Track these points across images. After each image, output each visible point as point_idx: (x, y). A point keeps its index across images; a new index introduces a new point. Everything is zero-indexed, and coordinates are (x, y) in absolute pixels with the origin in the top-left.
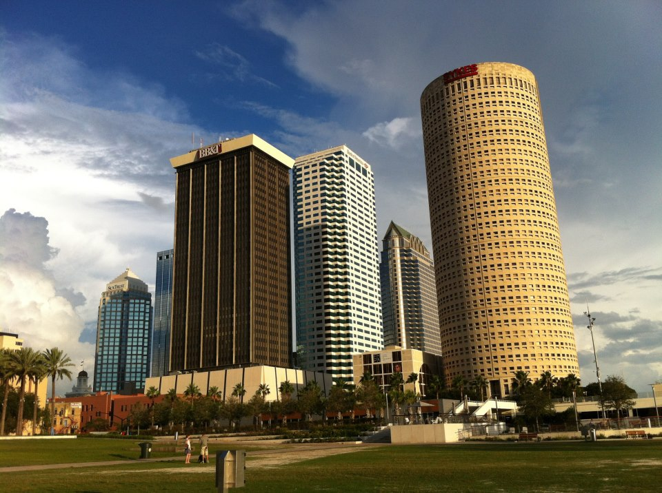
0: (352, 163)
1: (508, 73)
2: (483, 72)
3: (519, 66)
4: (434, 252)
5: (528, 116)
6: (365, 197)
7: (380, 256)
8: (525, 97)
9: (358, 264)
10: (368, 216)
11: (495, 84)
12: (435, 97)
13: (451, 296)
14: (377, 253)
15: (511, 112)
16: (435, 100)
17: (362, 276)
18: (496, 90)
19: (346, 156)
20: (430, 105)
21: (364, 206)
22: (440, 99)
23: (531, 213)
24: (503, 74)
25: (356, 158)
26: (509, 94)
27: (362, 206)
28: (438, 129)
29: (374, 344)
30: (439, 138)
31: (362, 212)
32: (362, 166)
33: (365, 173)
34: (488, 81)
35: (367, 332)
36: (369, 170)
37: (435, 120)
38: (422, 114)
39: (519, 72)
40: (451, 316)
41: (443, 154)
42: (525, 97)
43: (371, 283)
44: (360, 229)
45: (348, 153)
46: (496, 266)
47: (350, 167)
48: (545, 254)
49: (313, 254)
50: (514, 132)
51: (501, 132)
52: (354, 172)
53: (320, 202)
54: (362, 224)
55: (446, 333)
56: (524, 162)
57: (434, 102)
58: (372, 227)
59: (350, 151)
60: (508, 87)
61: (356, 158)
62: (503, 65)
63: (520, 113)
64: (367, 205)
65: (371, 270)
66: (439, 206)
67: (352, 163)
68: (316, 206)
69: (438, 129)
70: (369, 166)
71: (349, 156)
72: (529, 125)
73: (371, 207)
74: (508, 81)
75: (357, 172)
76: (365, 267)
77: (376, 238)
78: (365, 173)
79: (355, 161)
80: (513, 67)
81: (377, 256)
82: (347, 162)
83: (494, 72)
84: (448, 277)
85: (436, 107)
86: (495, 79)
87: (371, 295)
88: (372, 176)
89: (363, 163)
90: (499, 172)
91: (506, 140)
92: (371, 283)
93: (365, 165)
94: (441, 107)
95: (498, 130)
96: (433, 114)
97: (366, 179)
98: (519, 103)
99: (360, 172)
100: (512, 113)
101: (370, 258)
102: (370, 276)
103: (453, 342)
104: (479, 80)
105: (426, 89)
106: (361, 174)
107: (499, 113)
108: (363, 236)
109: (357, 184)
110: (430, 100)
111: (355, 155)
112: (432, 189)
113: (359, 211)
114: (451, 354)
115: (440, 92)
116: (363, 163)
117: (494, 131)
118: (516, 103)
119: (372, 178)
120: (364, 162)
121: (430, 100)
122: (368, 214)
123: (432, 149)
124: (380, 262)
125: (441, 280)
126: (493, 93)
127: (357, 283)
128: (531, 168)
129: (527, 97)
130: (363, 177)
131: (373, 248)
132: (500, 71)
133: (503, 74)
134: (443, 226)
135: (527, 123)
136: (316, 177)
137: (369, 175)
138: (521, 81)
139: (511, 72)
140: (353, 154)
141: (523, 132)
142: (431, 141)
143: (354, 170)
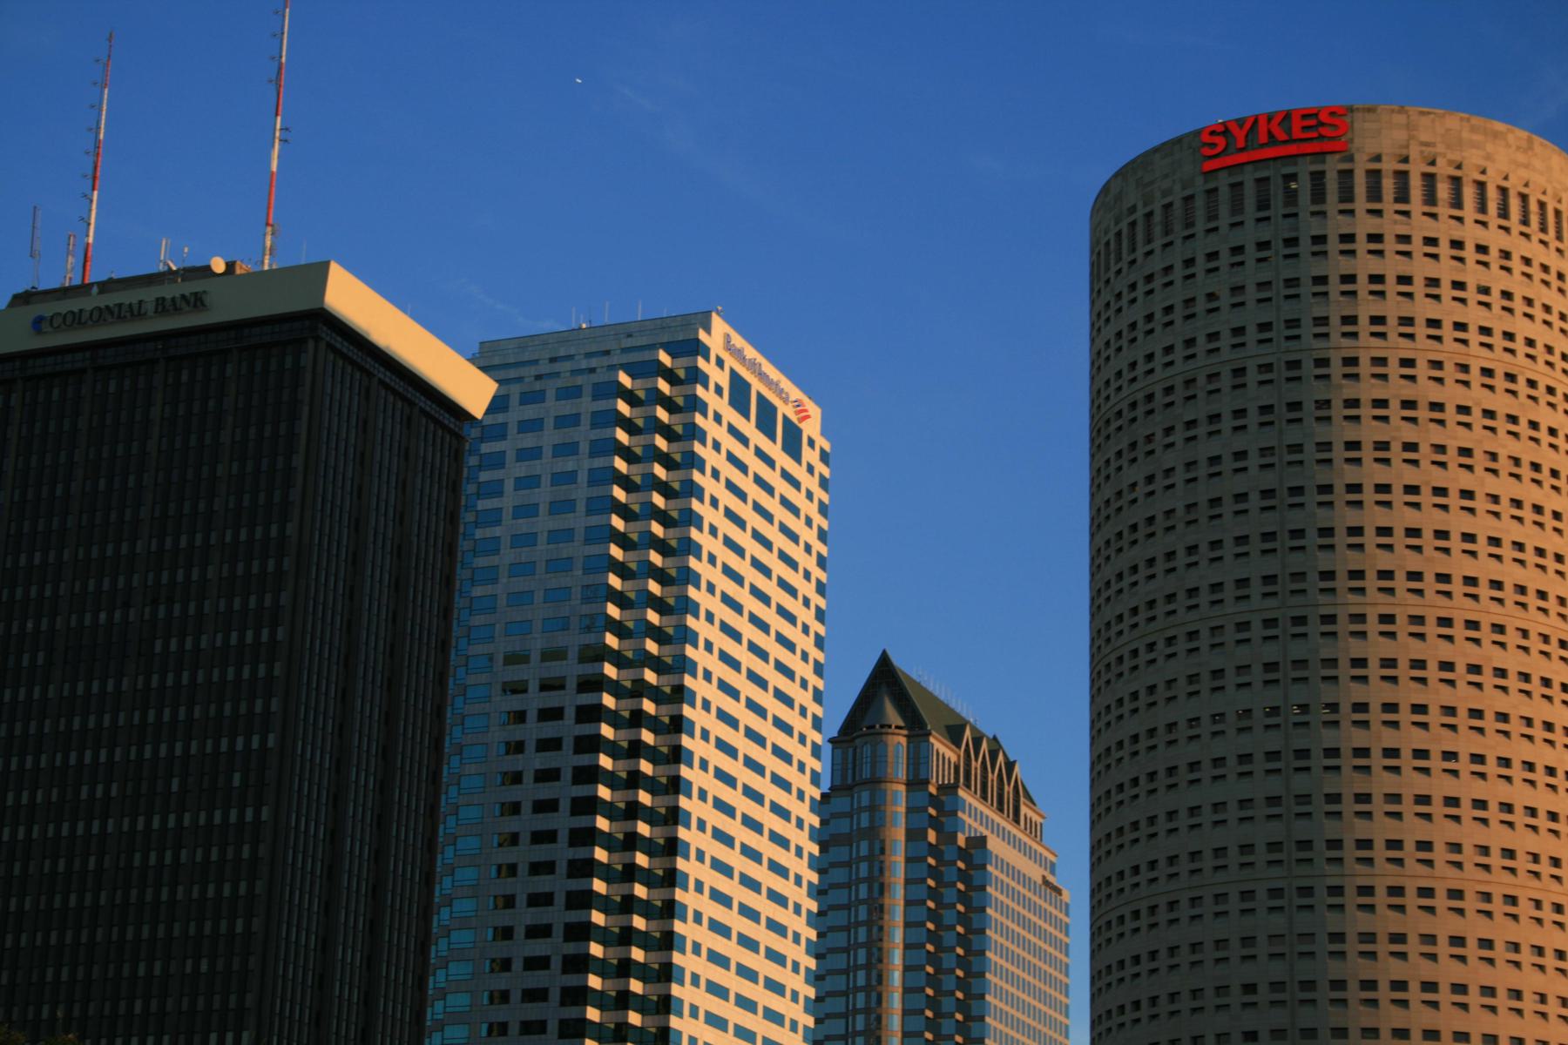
0: (739, 393)
1: (1473, 158)
2: (1371, 147)
3: (1524, 134)
4: (1095, 977)
5: (1539, 351)
6: (785, 502)
7: (827, 750)
8: (1535, 271)
9: (731, 751)
10: (795, 511)
11: (1416, 204)
12: (1157, 218)
13: (1153, 955)
14: (818, 738)
15: (1473, 328)
16: (1158, 230)
17: (741, 894)
18: (1420, 227)
19: (720, 363)
20: (1119, 259)
21: (779, 569)
22: (1179, 231)
23: (1517, 772)
24: (1450, 162)
25: (763, 377)
26: (1469, 253)
27: (770, 490)
28: (1160, 359)
29: (779, 884)
30: (1160, 399)
31: (766, 572)
32: (784, 410)
33: (793, 445)
34: (1388, 185)
35: (748, 943)
36: (811, 428)
37: (1149, 318)
38: (1095, 275)
39: (1521, 158)
40: (1143, 906)
41: (1169, 472)
42: (1535, 271)
43: (781, 871)
44: (757, 536)
45: (728, 346)
46: (1393, 363)
47: (731, 416)
48: (1543, 998)
49: (516, 996)
50: (1476, 418)
51: (1423, 413)
52: (744, 441)
53: (570, 713)
54: (767, 544)
55: (1116, 975)
56: (1507, 551)
57: (1149, 241)
58: (807, 589)
59: (738, 341)
60: (1469, 221)
61: (763, 377)
62: (1453, 121)
63: (1509, 336)
64: (795, 511)
65: (781, 871)
66: (1133, 326)
67: (739, 393)
68: (546, 791)
69: (1160, 359)
70: (814, 411)
71: (730, 363)
72: (1540, 392)
73: (808, 549)
74: (1469, 193)
75: (758, 438)
76: (760, 740)
77: (818, 697)
78: (793, 445)
79: (756, 386)
80: (1496, 135)
81: (816, 751)
82: (719, 390)
83: (1414, 153)
84: (1143, 572)
85: (1156, 264)
86: (1416, 185)
87: (777, 839)
88: (825, 457)
89: (789, 398)
90: (1400, 583)
91: (1441, 449)
92: (783, 814)
93: (798, 404)
94: (1178, 266)
95: (1409, 404)
96: (1142, 288)
97: (799, 472)
98: (1507, 295)
99: (772, 437)
100: (1473, 336)
101: (786, 728)
102: (774, 926)
103: (1144, 921)
104: (1347, 175)
105: (1121, 174)
106: (775, 450)
107: (1421, 330)
108: (763, 655)
109: (754, 492)
110: (1133, 224)
111: (760, 359)
112: (1109, 572)
113: (759, 480)
114: (1129, 1015)
115: (1178, 204)
116: (789, 398)
117: (1395, 404)
118: (1496, 293)
119: (821, 468)
120: (795, 393)
121: (1133, 224)
122: (795, 579)
123: (1124, 445)
124: (826, 785)
125: (1116, 798)
126: (1405, 239)
127: (720, 805)
128: (1533, 579)
129: (1545, 268)
130: (783, 460)
131: (804, 684)
132: (1440, 148)
133: (1450, 162)
134: (1144, 698)
135: (1532, 384)
136: (548, 837)
137: (810, 456)
138: (1524, 198)
139: (1488, 157)
140: (751, 353)
141: (1513, 419)
142: (1124, 405)
143: (748, 428)
